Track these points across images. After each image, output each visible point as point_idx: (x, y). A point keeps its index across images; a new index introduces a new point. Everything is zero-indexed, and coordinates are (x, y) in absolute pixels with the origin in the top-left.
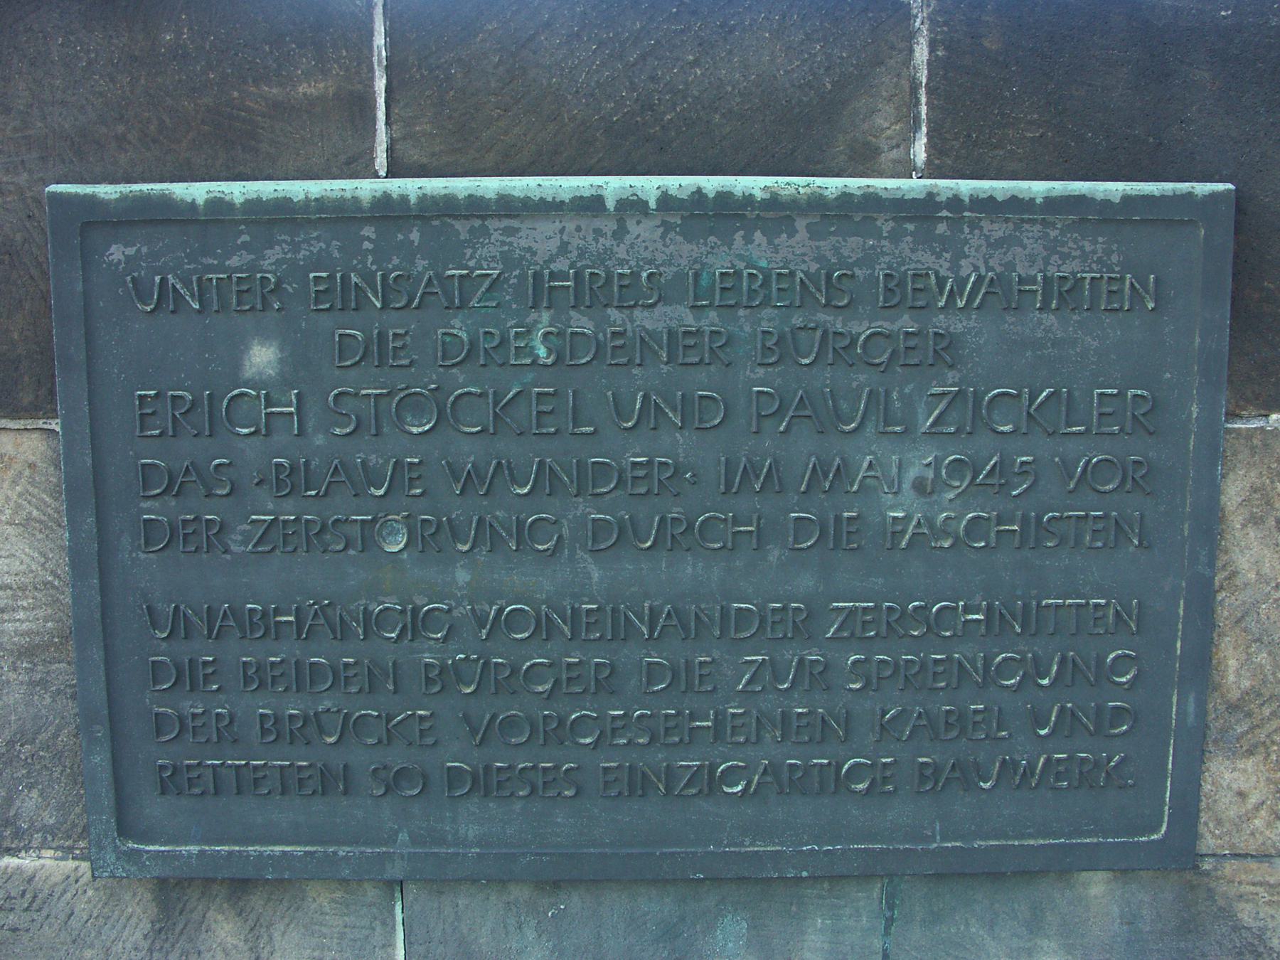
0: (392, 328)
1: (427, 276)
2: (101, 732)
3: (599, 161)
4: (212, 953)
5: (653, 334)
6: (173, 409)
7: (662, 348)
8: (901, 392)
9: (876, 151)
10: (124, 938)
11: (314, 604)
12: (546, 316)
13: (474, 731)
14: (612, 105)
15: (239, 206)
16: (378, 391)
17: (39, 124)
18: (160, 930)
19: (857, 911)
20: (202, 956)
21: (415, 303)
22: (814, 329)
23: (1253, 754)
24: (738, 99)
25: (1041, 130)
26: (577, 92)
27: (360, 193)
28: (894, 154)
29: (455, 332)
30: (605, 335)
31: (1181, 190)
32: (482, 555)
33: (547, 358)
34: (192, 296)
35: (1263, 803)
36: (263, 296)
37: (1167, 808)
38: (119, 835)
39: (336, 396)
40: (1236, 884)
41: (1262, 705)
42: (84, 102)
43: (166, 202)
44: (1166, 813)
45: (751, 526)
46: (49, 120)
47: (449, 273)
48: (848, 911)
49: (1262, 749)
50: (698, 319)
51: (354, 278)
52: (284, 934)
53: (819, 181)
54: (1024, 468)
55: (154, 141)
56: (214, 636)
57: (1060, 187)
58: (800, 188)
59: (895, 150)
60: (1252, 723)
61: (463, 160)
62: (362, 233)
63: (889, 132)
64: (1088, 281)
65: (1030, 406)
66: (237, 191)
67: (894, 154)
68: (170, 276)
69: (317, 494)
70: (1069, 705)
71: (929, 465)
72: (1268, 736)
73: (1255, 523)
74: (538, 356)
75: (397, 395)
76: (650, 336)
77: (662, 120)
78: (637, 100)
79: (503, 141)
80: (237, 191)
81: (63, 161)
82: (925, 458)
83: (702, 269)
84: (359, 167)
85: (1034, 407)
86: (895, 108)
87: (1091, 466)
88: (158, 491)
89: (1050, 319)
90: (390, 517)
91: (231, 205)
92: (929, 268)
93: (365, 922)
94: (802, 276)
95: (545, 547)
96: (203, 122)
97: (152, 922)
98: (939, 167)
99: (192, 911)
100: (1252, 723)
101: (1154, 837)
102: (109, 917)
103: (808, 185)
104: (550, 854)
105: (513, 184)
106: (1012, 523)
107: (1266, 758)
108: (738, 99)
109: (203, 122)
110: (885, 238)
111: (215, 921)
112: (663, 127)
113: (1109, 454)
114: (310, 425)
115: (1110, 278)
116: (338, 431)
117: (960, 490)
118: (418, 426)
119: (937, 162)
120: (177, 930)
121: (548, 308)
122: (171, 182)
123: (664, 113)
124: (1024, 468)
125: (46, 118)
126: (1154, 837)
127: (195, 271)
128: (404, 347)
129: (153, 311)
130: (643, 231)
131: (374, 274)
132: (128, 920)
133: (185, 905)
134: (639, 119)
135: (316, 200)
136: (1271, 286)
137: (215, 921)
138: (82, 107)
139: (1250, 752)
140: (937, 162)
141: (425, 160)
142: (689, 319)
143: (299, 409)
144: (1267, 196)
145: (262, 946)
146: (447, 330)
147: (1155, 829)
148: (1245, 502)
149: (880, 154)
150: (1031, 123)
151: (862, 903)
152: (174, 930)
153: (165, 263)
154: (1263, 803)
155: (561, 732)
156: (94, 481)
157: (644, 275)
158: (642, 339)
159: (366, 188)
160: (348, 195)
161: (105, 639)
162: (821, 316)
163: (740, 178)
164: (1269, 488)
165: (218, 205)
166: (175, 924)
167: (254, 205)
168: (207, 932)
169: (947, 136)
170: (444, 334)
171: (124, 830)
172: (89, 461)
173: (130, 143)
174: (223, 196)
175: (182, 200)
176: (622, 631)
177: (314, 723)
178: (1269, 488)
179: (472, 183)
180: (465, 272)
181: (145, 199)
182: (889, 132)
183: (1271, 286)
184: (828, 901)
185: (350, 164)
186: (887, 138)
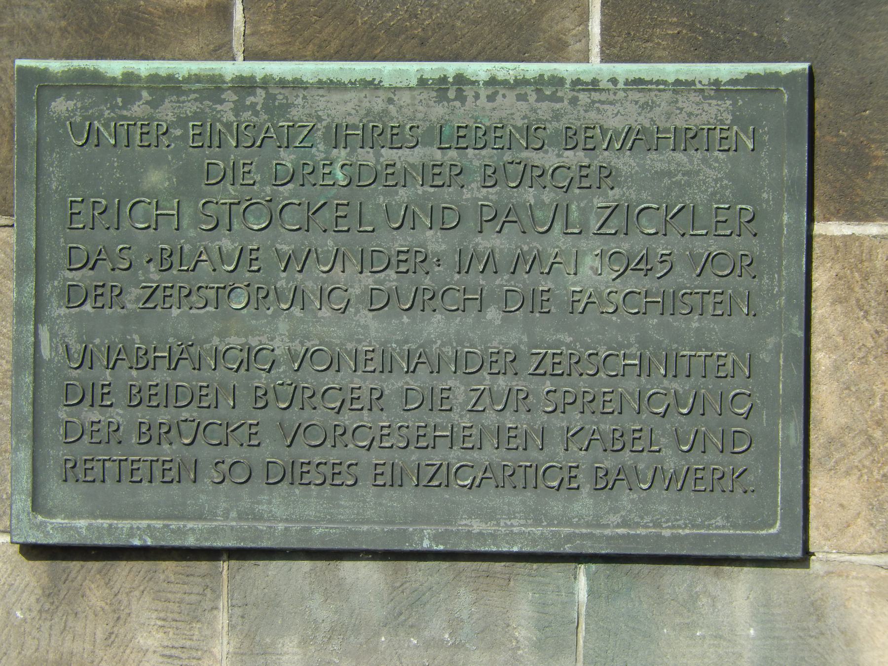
0: (242, 159)
1: (267, 126)
2: (27, 433)
3: (381, 51)
4: (85, 614)
5: (412, 166)
6: (94, 209)
7: (419, 175)
8: (578, 206)
9: (566, 45)
10: (22, 601)
11: (182, 344)
12: (343, 153)
13: (285, 436)
14: (390, 14)
15: (121, 77)
16: (232, 201)
17: (9, 20)
18: (49, 595)
19: (558, 587)
20: (78, 616)
21: (258, 144)
22: (520, 163)
23: (850, 475)
24: (473, 11)
25: (679, 29)
26: (367, 5)
27: (223, 72)
28: (578, 46)
29: (284, 163)
30: (382, 167)
31: (770, 69)
32: (296, 311)
33: (344, 181)
34: (110, 135)
35: (859, 514)
36: (158, 137)
37: (779, 509)
38: (33, 511)
39: (204, 204)
40: (844, 577)
41: (854, 437)
42: (40, 6)
43: (96, 75)
44: (779, 512)
45: (477, 295)
46: (16, 17)
47: (281, 124)
48: (551, 588)
49: (856, 471)
50: (444, 155)
51: (218, 126)
52: (139, 599)
53: (523, 66)
54: (664, 258)
55: (86, 32)
56: (111, 366)
57: (686, 68)
58: (510, 72)
59: (578, 44)
60: (847, 451)
61: (292, 49)
62: (512, 82)
63: (574, 32)
64: (706, 131)
65: (666, 216)
66: (143, 68)
67: (578, 46)
68: (96, 122)
69: (188, 269)
70: (703, 429)
71: (597, 255)
72: (860, 461)
73: (841, 302)
74: (338, 180)
75: (244, 203)
76: (411, 167)
77: (423, 24)
78: (407, 11)
79: (318, 37)
80: (143, 68)
81: (24, 44)
82: (595, 250)
83: (446, 124)
84: (222, 52)
85: (670, 216)
86: (579, 16)
87: (711, 257)
88: (80, 266)
89: (679, 156)
90: (236, 285)
91: (138, 78)
92: (597, 123)
93: (196, 589)
94: (511, 128)
95: (339, 307)
96: (119, 20)
97: (43, 589)
98: (608, 55)
99: (72, 581)
100: (847, 451)
101: (772, 531)
102: (13, 585)
103: (515, 69)
104: (336, 528)
105: (327, 67)
106: (657, 296)
107: (859, 479)
108: (473, 11)
109: (119, 20)
110: (453, 100)
111: (90, 589)
112: (423, 29)
113: (724, 249)
114: (185, 223)
115: (721, 129)
116: (204, 227)
117: (620, 273)
118: (257, 225)
119: (607, 52)
120: (62, 596)
121: (345, 148)
122: (97, 59)
123: (425, 20)
124: (664, 258)
125: (14, 16)
126: (772, 531)
127: (112, 119)
128: (249, 172)
129: (82, 145)
130: (688, 102)
131: (232, 123)
132: (26, 587)
133: (68, 575)
134: (408, 24)
135: (195, 75)
136: (845, 134)
137: (90, 589)
138: (39, 9)
139: (847, 473)
140: (607, 52)
141: (266, 49)
142: (438, 155)
143: (178, 212)
144: (838, 72)
145: (122, 608)
146: (279, 162)
147: (772, 526)
148: (832, 287)
149: (568, 46)
150: (671, 24)
151: (561, 582)
152: (58, 595)
153: (92, 113)
154: (859, 514)
155: (338, 435)
156: (36, 259)
157: (408, 127)
158: (405, 169)
159: (229, 69)
160: (217, 73)
161: (34, 368)
162: (525, 154)
163: (471, 64)
164: (849, 277)
165: (129, 77)
166: (59, 591)
167: (154, 78)
168: (83, 597)
169: (615, 34)
170: (277, 164)
171: (36, 507)
172: (34, 245)
173: (69, 33)
174: (378, 104)
175: (63, 72)
176: (387, 366)
177: (172, 429)
178: (849, 277)
179: (297, 66)
180: (291, 124)
181: (81, 73)
182: (574, 32)
183: (845, 134)
184: (537, 578)
185: (216, 50)
186: (573, 36)
